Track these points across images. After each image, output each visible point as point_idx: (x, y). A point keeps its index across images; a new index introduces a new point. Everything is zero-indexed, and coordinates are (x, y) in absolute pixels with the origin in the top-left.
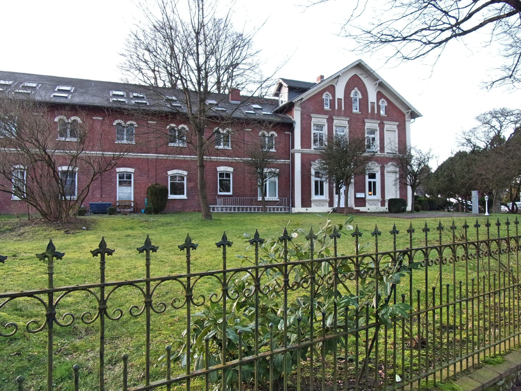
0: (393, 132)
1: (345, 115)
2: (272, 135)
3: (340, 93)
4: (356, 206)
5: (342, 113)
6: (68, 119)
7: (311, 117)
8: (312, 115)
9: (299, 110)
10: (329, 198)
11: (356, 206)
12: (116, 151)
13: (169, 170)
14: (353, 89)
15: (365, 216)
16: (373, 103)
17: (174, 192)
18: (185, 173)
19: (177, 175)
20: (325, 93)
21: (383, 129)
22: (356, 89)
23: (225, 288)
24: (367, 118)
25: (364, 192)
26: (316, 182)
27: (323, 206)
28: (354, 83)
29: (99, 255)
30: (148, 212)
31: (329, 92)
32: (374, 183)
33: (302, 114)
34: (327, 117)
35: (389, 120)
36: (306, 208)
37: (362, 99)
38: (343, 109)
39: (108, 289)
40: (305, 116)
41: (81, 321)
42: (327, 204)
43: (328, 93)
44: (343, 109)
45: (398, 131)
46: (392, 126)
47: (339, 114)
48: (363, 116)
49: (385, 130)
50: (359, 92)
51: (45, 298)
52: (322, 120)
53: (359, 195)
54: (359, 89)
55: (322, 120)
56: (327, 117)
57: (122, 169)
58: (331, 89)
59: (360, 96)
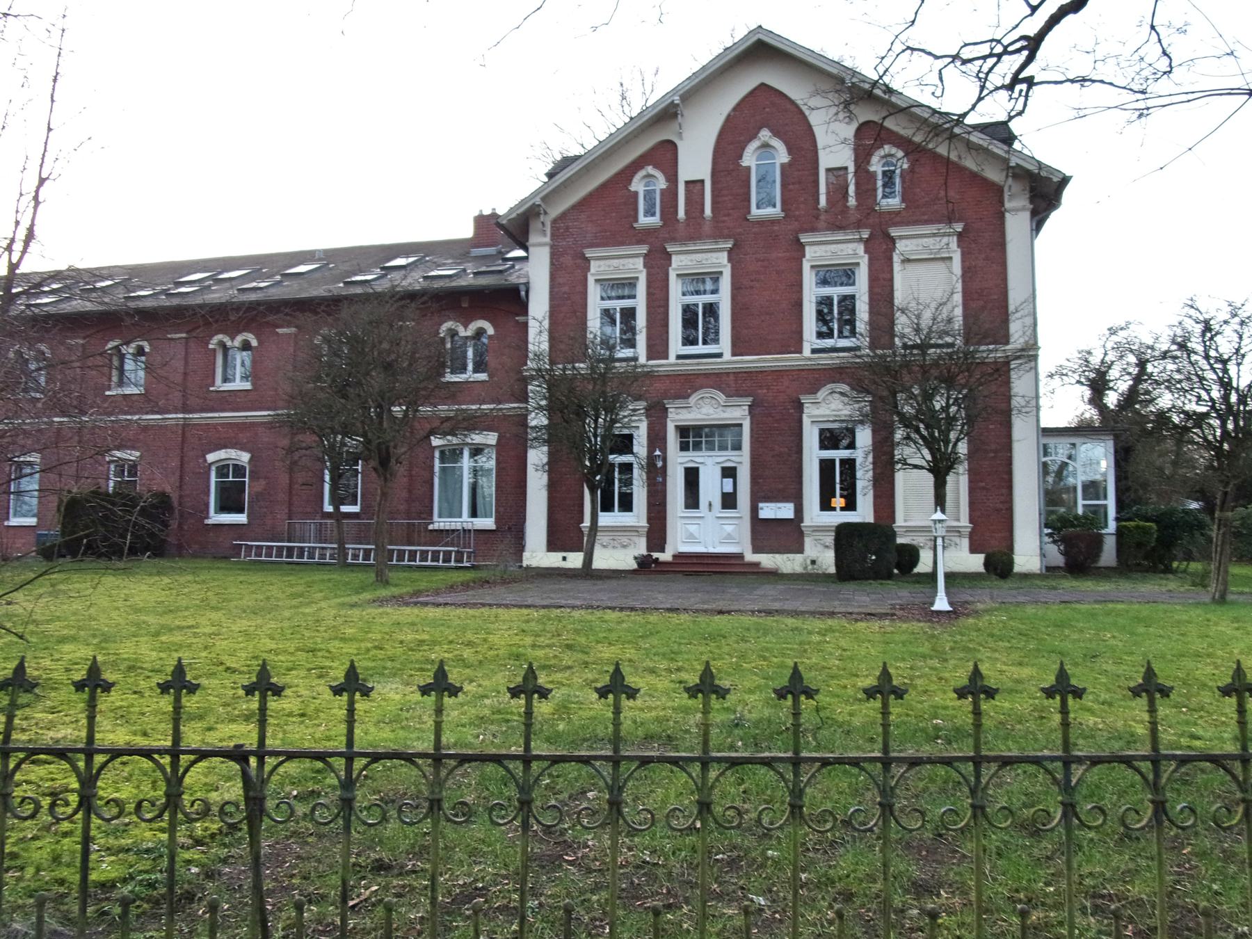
0: (941, 266)
1: (718, 233)
2: (480, 333)
3: (696, 161)
4: (756, 550)
5: (707, 228)
6: (233, 339)
7: (588, 260)
8: (589, 253)
9: (1023, 209)
10: (649, 520)
11: (756, 550)
12: (484, 402)
13: (210, 452)
14: (754, 136)
15: (263, 570)
16: (837, 173)
17: (223, 508)
18: (245, 457)
19: (230, 462)
20: (642, 173)
21: (890, 259)
22: (765, 134)
23: (525, 797)
24: (813, 230)
25: (796, 498)
26: (826, 467)
27: (624, 547)
28: (764, 112)
29: (789, 696)
30: (48, 553)
31: (656, 166)
32: (849, 465)
33: (555, 256)
34: (644, 249)
35: (908, 223)
36: (560, 555)
37: (790, 164)
38: (708, 211)
39: (359, 763)
40: (567, 260)
41: (135, 818)
42: (965, 542)
43: (650, 169)
44: (708, 211)
45: (963, 254)
46: (615, 262)
47: (694, 231)
48: (796, 225)
49: (896, 258)
50: (778, 144)
51: (166, 760)
52: (630, 263)
53: (769, 511)
54: (776, 133)
55: (630, 263)
56: (644, 249)
57: (221, 454)
58: (666, 156)
59: (782, 155)
